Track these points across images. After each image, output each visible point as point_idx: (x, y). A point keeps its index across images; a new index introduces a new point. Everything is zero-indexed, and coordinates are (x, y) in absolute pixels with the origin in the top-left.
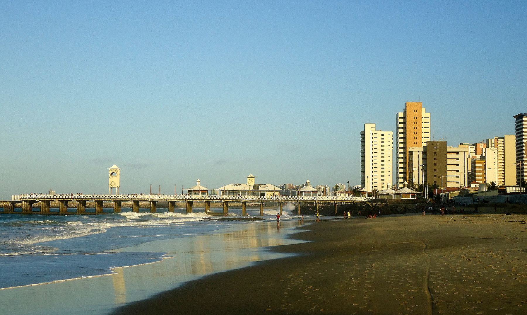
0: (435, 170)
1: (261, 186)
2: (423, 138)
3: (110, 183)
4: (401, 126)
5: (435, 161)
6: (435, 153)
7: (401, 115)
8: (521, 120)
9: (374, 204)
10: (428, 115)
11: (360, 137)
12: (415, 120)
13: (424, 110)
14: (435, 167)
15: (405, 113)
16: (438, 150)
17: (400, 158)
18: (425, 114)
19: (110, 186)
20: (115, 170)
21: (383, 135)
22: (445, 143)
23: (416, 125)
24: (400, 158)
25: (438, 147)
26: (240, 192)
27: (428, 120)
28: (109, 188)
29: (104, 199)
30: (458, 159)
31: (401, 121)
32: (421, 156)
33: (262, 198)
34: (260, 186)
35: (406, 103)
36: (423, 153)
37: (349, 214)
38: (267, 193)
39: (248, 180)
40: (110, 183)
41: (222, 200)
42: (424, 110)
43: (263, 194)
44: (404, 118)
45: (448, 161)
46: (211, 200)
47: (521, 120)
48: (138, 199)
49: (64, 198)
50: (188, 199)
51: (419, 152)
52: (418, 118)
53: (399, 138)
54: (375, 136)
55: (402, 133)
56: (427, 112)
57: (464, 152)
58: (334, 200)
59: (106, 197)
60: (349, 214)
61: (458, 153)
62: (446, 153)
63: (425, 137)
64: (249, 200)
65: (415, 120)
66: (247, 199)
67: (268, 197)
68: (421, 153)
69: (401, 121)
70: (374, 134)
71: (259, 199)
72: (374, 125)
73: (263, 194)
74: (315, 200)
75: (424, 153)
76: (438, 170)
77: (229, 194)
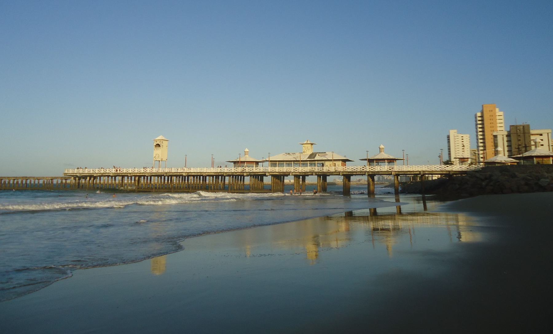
1: (319, 154)
3: (154, 156)
7: (479, 114)
10: (501, 113)
11: (446, 139)
13: (497, 110)
15: (482, 113)
17: (480, 146)
18: (499, 113)
19: (154, 159)
20: (160, 141)
21: (462, 137)
22: (528, 126)
23: (492, 121)
24: (480, 146)
27: (502, 117)
28: (154, 161)
29: (139, 173)
31: (480, 119)
32: (506, 139)
33: (350, 169)
34: (317, 155)
35: (483, 106)
36: (507, 136)
37: (448, 178)
38: (327, 163)
39: (304, 148)
40: (154, 156)
41: (266, 172)
42: (497, 110)
44: (482, 116)
50: (292, 172)
51: (503, 135)
52: (493, 117)
53: (479, 132)
54: (457, 137)
56: (500, 111)
57: (548, 133)
60: (448, 178)
61: (541, 135)
62: (530, 135)
64: (300, 173)
66: (297, 172)
69: (480, 119)
72: (456, 131)
74: (390, 170)
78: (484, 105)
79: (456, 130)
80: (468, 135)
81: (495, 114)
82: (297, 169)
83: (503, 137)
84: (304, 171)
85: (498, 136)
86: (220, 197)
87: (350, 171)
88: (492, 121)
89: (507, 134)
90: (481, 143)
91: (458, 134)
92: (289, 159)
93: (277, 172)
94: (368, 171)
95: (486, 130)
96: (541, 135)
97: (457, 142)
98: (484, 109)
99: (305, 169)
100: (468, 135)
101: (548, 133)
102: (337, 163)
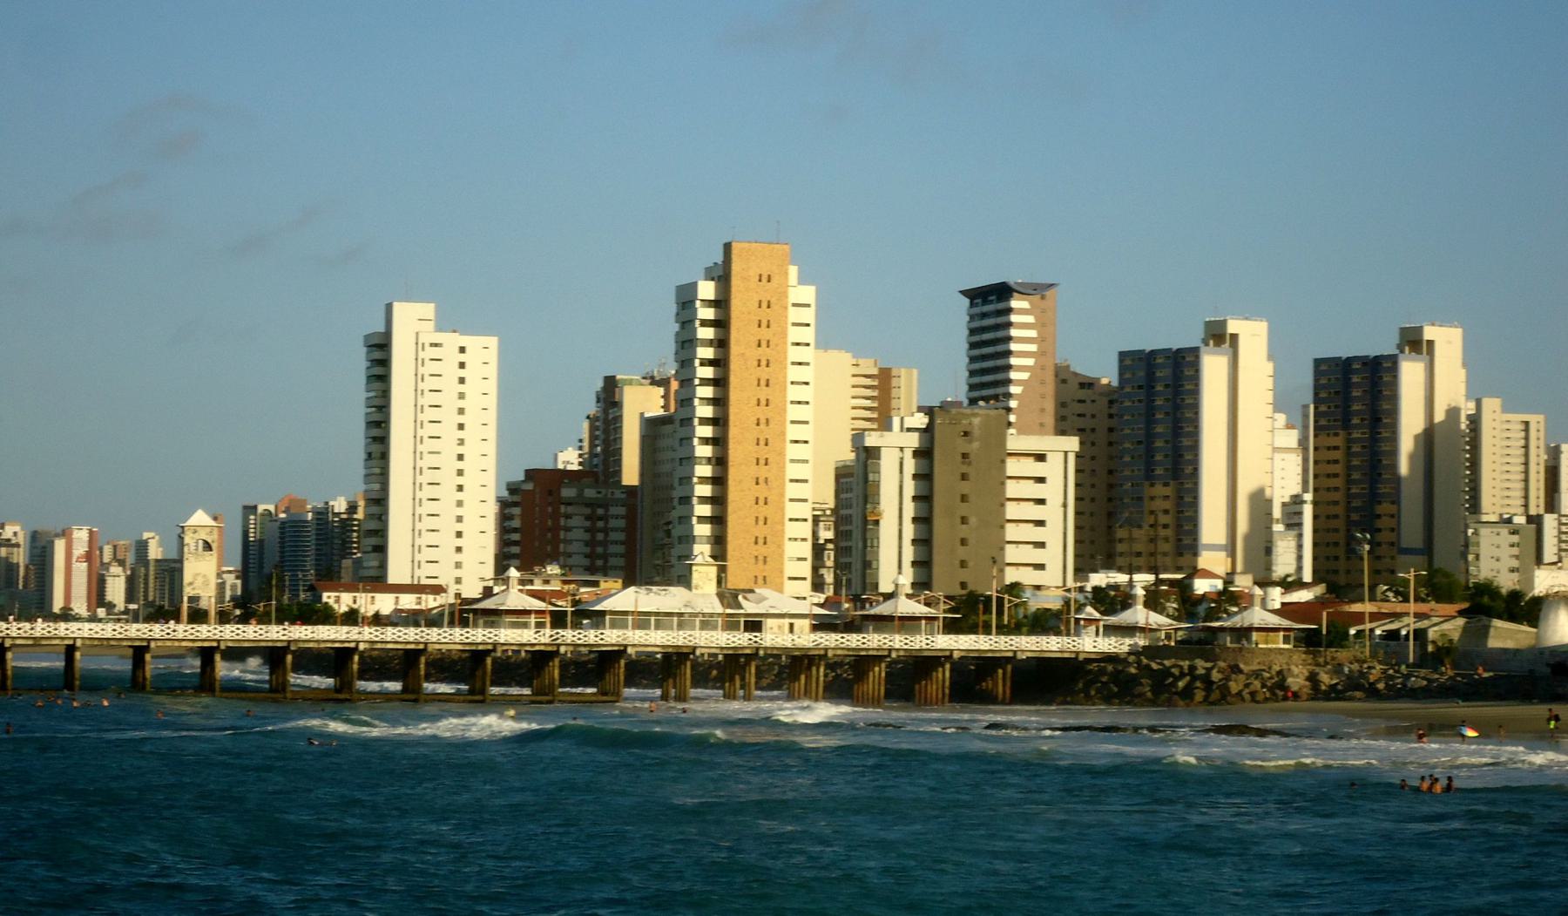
0: (964, 520)
2: (1088, 415)
4: (706, 333)
5: (965, 487)
6: (965, 456)
8: (1001, 306)
9: (1186, 667)
10: (807, 293)
12: (764, 314)
14: (963, 509)
16: (976, 445)
25: (976, 432)
26: (720, 619)
30: (1041, 480)
32: (910, 466)
36: (917, 454)
38: (770, 623)
43: (754, 625)
44: (721, 303)
45: (1010, 484)
46: (585, 645)
47: (1001, 306)
48: (317, 641)
49: (38, 635)
54: (435, 352)
55: (710, 363)
56: (802, 281)
57: (1066, 453)
58: (1014, 648)
59: (198, 634)
61: (1041, 457)
63: (804, 386)
65: (764, 314)
67: (774, 637)
68: (908, 454)
70: (432, 345)
71: (755, 645)
72: (428, 310)
73: (754, 625)
75: (924, 454)
76: (973, 520)
77: (681, 626)
78: (736, 248)
79: (431, 306)
80: (493, 342)
81: (785, 295)
82: (713, 639)
83: (902, 458)
84: (733, 645)
85: (884, 452)
86: (809, 741)
87: (854, 646)
88: (765, 334)
89: (917, 446)
90: (705, 441)
91: (439, 329)
92: (675, 608)
93: (658, 646)
94: (897, 647)
95: (734, 380)
96: (1041, 457)
97: (431, 383)
98: (736, 267)
99: (735, 639)
100: (493, 342)
101: (1066, 453)
102: (798, 623)
